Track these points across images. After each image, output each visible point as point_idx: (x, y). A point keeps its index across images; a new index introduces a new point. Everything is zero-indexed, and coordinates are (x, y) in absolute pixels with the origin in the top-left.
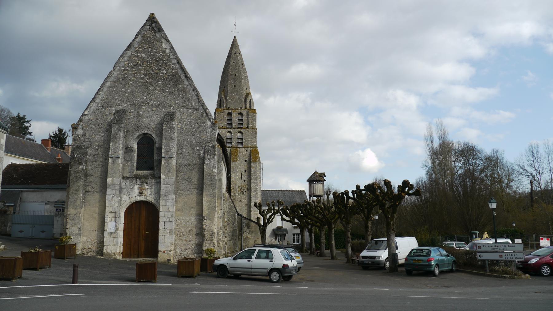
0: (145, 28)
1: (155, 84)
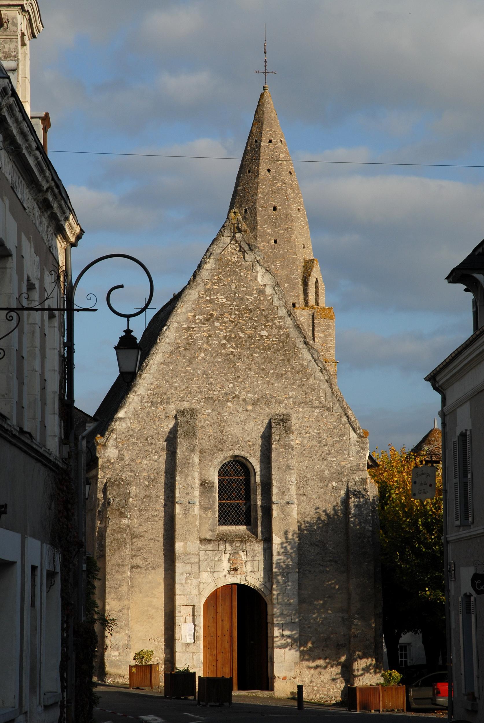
0: (222, 241)
1: (248, 358)
